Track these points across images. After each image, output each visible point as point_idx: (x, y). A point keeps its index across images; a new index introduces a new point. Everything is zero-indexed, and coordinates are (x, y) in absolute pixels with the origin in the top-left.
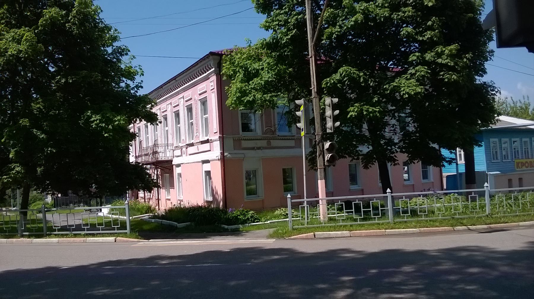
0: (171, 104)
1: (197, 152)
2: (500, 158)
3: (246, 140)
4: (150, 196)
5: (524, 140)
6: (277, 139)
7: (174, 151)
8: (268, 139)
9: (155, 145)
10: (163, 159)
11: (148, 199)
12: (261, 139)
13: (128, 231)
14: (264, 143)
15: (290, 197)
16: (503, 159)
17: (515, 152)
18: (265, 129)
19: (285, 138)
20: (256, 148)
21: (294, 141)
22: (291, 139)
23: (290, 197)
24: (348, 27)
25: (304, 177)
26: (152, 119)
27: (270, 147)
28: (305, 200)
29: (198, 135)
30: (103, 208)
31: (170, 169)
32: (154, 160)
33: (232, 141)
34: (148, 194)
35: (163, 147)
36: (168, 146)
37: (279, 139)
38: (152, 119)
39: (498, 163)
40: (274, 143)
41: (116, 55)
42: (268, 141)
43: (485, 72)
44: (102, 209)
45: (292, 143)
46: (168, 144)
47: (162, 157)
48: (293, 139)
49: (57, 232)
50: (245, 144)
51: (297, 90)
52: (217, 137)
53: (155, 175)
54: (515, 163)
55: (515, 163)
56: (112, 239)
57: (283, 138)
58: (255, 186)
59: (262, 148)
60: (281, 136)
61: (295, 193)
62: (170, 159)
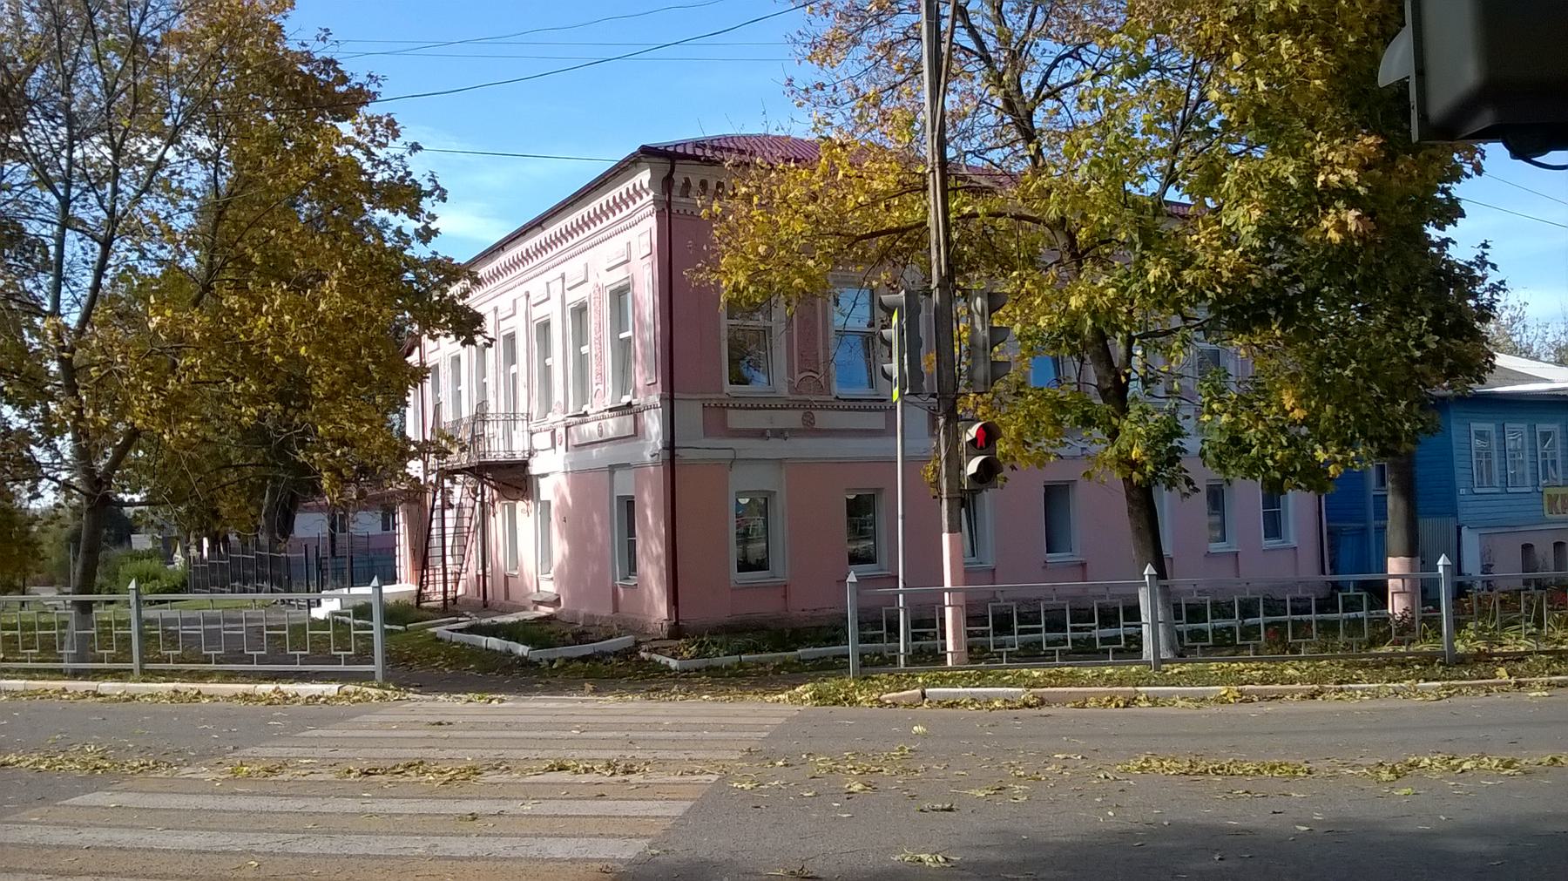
0: (563, 276)
1: (600, 439)
2: (1501, 482)
3: (740, 408)
4: (462, 565)
5: (1541, 427)
6: (832, 409)
7: (532, 434)
8: (807, 408)
9: (481, 416)
10: (501, 457)
11: (455, 573)
12: (788, 408)
13: (377, 667)
14: (793, 419)
15: (855, 580)
16: (1509, 485)
17: (1545, 463)
18: (798, 377)
19: (857, 404)
20: (768, 433)
21: (882, 415)
22: (876, 410)
23: (855, 580)
24: (274, 86)
25: (900, 521)
26: (467, 325)
27: (809, 430)
28: (901, 592)
29: (602, 389)
30: (326, 597)
31: (520, 489)
32: (475, 461)
33: (697, 408)
34: (454, 560)
35: (501, 423)
36: (515, 420)
37: (838, 409)
38: (467, 325)
39: (1494, 497)
40: (823, 419)
41: (1163, 53)
42: (805, 415)
43: (1463, 215)
44: (323, 600)
45: (876, 421)
46: (514, 414)
47: (497, 450)
48: (880, 410)
49: (213, 665)
50: (737, 419)
51: (1338, 231)
52: (655, 399)
53: (477, 504)
54: (1545, 498)
55: (1545, 498)
56: (332, 689)
57: (852, 404)
58: (764, 544)
59: (787, 434)
60: (845, 400)
61: (881, 570)
62: (519, 457)
